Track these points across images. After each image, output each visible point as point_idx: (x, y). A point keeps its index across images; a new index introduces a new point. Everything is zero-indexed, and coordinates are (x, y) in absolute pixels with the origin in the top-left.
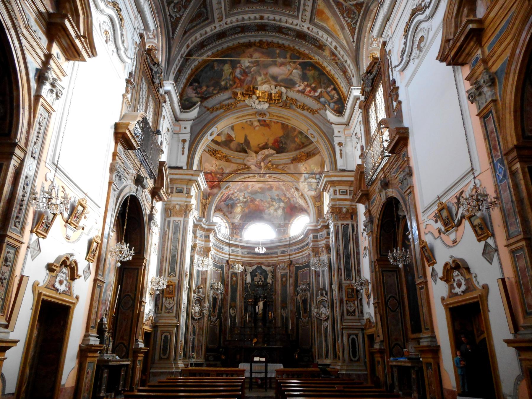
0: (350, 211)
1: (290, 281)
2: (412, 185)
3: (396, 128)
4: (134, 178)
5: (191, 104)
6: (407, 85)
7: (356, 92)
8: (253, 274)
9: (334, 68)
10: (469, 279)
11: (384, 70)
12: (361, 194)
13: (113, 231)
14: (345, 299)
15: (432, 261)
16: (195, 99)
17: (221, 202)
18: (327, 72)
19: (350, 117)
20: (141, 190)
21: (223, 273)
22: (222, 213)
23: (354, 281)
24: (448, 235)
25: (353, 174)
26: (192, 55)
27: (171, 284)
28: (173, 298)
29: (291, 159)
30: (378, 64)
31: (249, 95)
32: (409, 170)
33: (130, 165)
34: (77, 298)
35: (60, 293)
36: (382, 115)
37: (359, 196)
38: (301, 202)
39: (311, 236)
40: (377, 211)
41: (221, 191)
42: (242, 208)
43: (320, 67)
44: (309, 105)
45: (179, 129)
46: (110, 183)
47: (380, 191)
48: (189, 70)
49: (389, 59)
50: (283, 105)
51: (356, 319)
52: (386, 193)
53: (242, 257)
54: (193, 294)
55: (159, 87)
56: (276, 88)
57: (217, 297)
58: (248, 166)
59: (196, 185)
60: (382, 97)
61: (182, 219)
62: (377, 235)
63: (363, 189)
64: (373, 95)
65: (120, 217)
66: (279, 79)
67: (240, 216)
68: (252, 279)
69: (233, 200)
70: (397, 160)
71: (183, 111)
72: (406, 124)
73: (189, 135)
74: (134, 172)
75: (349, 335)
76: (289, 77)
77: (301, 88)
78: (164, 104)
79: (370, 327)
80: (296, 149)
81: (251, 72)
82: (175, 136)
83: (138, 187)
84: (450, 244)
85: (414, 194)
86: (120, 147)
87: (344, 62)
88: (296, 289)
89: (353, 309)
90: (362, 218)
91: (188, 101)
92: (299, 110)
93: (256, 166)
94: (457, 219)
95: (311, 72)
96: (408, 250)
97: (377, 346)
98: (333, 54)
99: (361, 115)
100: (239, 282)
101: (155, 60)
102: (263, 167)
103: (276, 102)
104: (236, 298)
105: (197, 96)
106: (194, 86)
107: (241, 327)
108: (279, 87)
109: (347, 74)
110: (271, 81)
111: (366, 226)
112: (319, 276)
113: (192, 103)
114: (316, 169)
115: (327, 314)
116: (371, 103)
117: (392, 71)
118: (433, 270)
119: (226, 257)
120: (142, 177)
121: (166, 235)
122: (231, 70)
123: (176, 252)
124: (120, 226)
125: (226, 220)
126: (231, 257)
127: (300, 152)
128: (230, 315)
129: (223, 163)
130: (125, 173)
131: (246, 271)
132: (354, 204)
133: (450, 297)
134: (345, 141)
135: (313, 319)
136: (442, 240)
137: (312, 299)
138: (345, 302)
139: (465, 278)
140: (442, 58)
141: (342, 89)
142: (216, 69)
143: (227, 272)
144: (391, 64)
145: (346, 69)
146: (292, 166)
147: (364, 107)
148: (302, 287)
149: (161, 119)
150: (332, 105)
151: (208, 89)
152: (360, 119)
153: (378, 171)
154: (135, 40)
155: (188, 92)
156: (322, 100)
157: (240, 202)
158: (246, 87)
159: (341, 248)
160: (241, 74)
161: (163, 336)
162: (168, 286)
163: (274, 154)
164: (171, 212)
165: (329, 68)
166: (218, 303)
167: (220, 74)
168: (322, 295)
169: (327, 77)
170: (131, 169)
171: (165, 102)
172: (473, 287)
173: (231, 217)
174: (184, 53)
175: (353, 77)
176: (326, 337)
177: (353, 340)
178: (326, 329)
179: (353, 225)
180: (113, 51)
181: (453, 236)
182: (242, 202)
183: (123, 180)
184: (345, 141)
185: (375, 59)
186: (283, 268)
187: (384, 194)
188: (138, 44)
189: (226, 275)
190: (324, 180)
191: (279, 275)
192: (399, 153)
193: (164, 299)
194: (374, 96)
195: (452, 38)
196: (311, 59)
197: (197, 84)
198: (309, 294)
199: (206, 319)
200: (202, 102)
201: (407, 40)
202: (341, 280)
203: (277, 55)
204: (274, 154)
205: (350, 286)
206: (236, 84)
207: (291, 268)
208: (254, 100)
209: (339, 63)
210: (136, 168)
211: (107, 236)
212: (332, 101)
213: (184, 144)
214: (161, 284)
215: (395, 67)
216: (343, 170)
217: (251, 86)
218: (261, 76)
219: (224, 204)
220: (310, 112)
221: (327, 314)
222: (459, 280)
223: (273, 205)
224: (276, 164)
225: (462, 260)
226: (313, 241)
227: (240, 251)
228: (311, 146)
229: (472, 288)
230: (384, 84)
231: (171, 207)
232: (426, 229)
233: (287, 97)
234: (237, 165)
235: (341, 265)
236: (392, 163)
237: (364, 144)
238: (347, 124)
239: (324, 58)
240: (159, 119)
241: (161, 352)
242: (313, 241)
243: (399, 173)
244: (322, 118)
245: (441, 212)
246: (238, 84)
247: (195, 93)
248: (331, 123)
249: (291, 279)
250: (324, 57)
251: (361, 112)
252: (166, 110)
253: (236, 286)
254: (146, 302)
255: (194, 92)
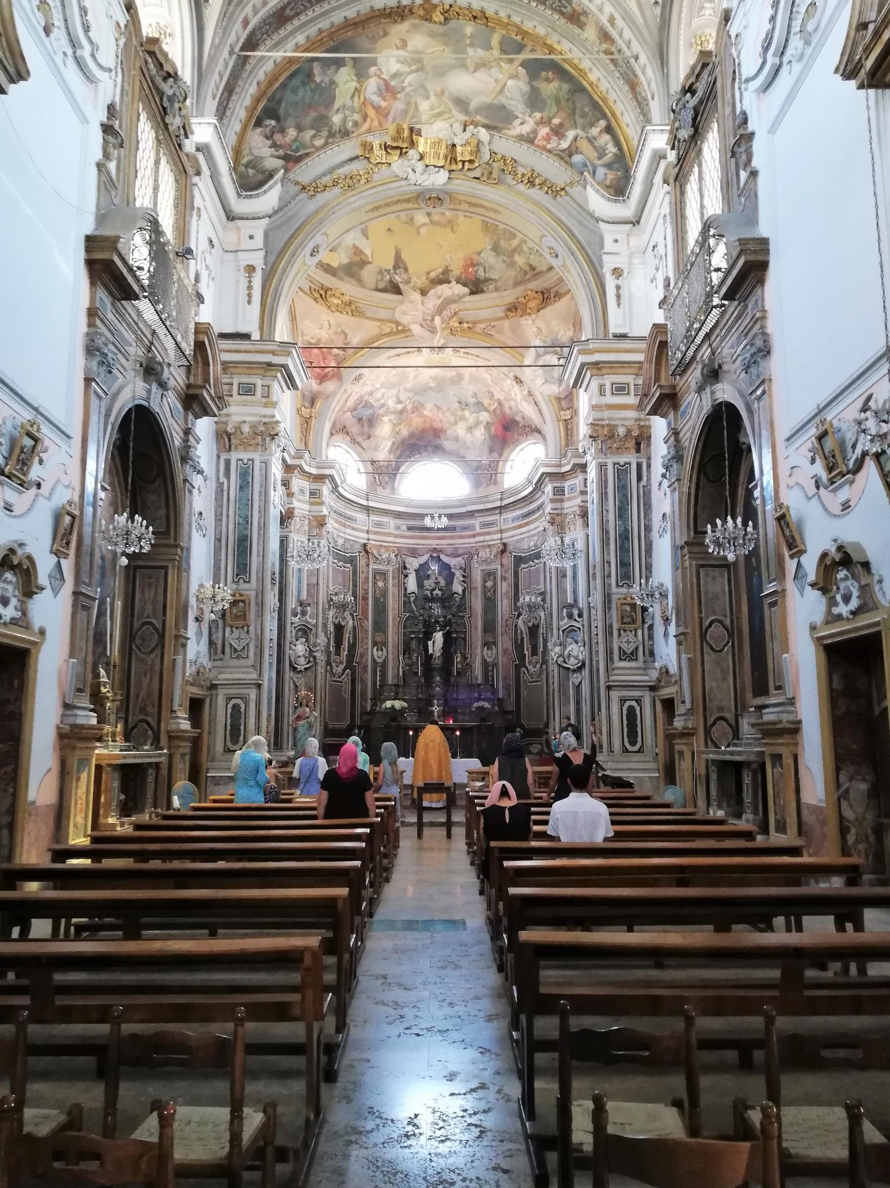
0: (635, 433)
1: (504, 588)
2: (767, 377)
3: (740, 240)
4: (141, 365)
5: (260, 177)
6: (772, 130)
7: (658, 140)
8: (421, 573)
9: (608, 73)
10: (868, 585)
11: (722, 87)
12: (658, 393)
13: (104, 489)
14: (615, 626)
15: (797, 546)
16: (272, 163)
17: (344, 412)
18: (591, 84)
19: (642, 204)
20: (159, 395)
21: (355, 573)
22: (348, 438)
23: (636, 588)
24: (835, 491)
25: (643, 345)
26: (258, 45)
27: (241, 598)
28: (246, 628)
29: (504, 308)
30: (709, 68)
31: (401, 149)
32: (765, 341)
33: (130, 336)
34: (42, 632)
35: (5, 624)
36: (714, 206)
37: (654, 399)
38: (528, 410)
39: (549, 488)
40: (692, 433)
41: (344, 387)
42: (395, 425)
43: (573, 71)
44: (545, 175)
45: (236, 241)
46: (88, 380)
47: (700, 389)
48: (251, 84)
49: (735, 56)
50: (483, 174)
51: (638, 668)
52: (713, 393)
53: (396, 536)
54: (289, 618)
55: (182, 137)
56: (465, 130)
57: (343, 624)
58: (404, 326)
59: (283, 376)
60: (717, 155)
61: (257, 457)
62: (690, 488)
63: (663, 382)
64: (697, 148)
65: (116, 453)
66: (473, 105)
67: (390, 444)
68: (420, 586)
69: (372, 407)
70: (739, 317)
71: (244, 193)
72: (764, 230)
73: (262, 254)
74: (140, 353)
75: (623, 701)
76: (496, 102)
77: (526, 129)
78: (196, 179)
79: (669, 684)
80: (516, 284)
81: (403, 89)
82: (230, 256)
83: (151, 386)
84: (836, 509)
85: (770, 396)
86: (102, 294)
87: (632, 61)
88: (515, 604)
89: (632, 647)
90: (660, 449)
91: (253, 168)
92: (522, 187)
93: (421, 325)
94: (855, 457)
95: (551, 85)
96: (750, 523)
97: (678, 723)
98: (605, 36)
99: (667, 199)
100: (392, 590)
101: (167, 68)
102: (439, 329)
103: (467, 165)
104: (386, 626)
105: (276, 154)
106: (266, 126)
107: (397, 686)
108: (472, 127)
109: (638, 89)
110: (454, 112)
111: (667, 467)
112: (565, 576)
113: (263, 172)
114: (562, 332)
115: (581, 657)
116: (691, 170)
117: (740, 88)
118: (799, 565)
119: (362, 537)
120: (160, 363)
121: (222, 491)
122: (355, 84)
123: (246, 529)
124: (118, 474)
125: (359, 456)
126: (371, 536)
127: (526, 290)
128: (374, 660)
129: (346, 319)
130: (120, 356)
131: (405, 568)
132: (643, 416)
133: (827, 623)
134: (630, 264)
135: (551, 667)
136: (821, 502)
137: (549, 626)
138: (615, 633)
139: (859, 583)
140: (849, 70)
141: (625, 129)
142: (318, 79)
143: (364, 569)
144: (739, 71)
145: (636, 76)
146: (506, 324)
147: (676, 180)
148: (526, 599)
149: (191, 217)
150: (601, 171)
151: (301, 134)
152: (666, 209)
153: (698, 340)
154: (115, 18)
155: (254, 144)
156: (577, 159)
157: (388, 412)
158: (392, 129)
159: (611, 517)
160: (380, 93)
161: (230, 706)
162: (234, 603)
163: (464, 296)
164: (230, 441)
165: (594, 75)
166: (346, 636)
167: (327, 94)
168: (570, 616)
169: (591, 98)
170: (130, 345)
171: (198, 173)
172: (874, 602)
173: (369, 448)
174: (237, 41)
175: (653, 99)
176: (578, 703)
177: (631, 710)
178: (578, 688)
179: (639, 466)
180: (65, 54)
181: (843, 494)
182: (393, 413)
183: (115, 371)
184: (630, 264)
185: (704, 54)
186: (486, 561)
187: (709, 395)
188: (122, 26)
189: (362, 576)
190: (578, 360)
191: (477, 576)
192: (744, 301)
193: (228, 630)
194: (699, 152)
195: (873, 18)
196: (551, 50)
197: (273, 123)
198: (542, 614)
199: (320, 670)
200: (287, 170)
201: (776, 12)
202: (610, 585)
203: (468, 42)
204: (464, 296)
205: (629, 599)
206: (369, 120)
207: (505, 561)
208: (413, 162)
209: (620, 62)
210: (142, 341)
211: (91, 499)
212: (600, 162)
213: (250, 277)
214: (218, 598)
215: (748, 80)
216: (623, 337)
217: (405, 126)
218: (428, 98)
219: (353, 417)
220: (547, 193)
221: (581, 657)
222: (848, 588)
223: (463, 418)
224: (468, 320)
225: (858, 546)
226: (552, 501)
227: (392, 526)
228: (551, 274)
229: (871, 605)
230: (721, 122)
231: (230, 429)
232: (790, 476)
233: (493, 153)
234: (378, 324)
235: (609, 554)
236: (730, 322)
237: (671, 274)
238: (636, 222)
239: (584, 47)
240: (187, 218)
241: (228, 738)
242: (552, 501)
243: (742, 346)
244: (575, 206)
245: (822, 441)
246: (373, 120)
247: (270, 147)
248: (598, 220)
249: (505, 585)
250: (583, 44)
251: (668, 193)
252: (203, 188)
253: (385, 599)
254: (189, 636)
255: (269, 143)
